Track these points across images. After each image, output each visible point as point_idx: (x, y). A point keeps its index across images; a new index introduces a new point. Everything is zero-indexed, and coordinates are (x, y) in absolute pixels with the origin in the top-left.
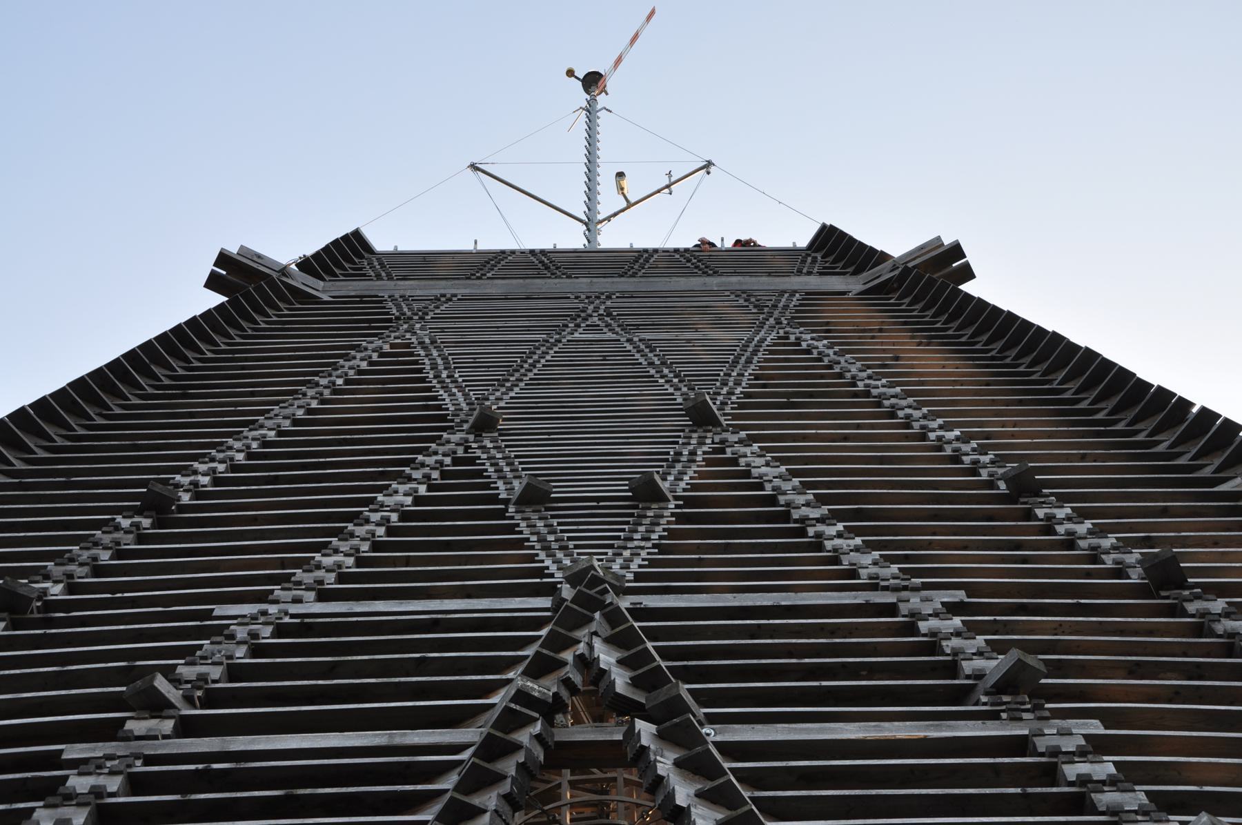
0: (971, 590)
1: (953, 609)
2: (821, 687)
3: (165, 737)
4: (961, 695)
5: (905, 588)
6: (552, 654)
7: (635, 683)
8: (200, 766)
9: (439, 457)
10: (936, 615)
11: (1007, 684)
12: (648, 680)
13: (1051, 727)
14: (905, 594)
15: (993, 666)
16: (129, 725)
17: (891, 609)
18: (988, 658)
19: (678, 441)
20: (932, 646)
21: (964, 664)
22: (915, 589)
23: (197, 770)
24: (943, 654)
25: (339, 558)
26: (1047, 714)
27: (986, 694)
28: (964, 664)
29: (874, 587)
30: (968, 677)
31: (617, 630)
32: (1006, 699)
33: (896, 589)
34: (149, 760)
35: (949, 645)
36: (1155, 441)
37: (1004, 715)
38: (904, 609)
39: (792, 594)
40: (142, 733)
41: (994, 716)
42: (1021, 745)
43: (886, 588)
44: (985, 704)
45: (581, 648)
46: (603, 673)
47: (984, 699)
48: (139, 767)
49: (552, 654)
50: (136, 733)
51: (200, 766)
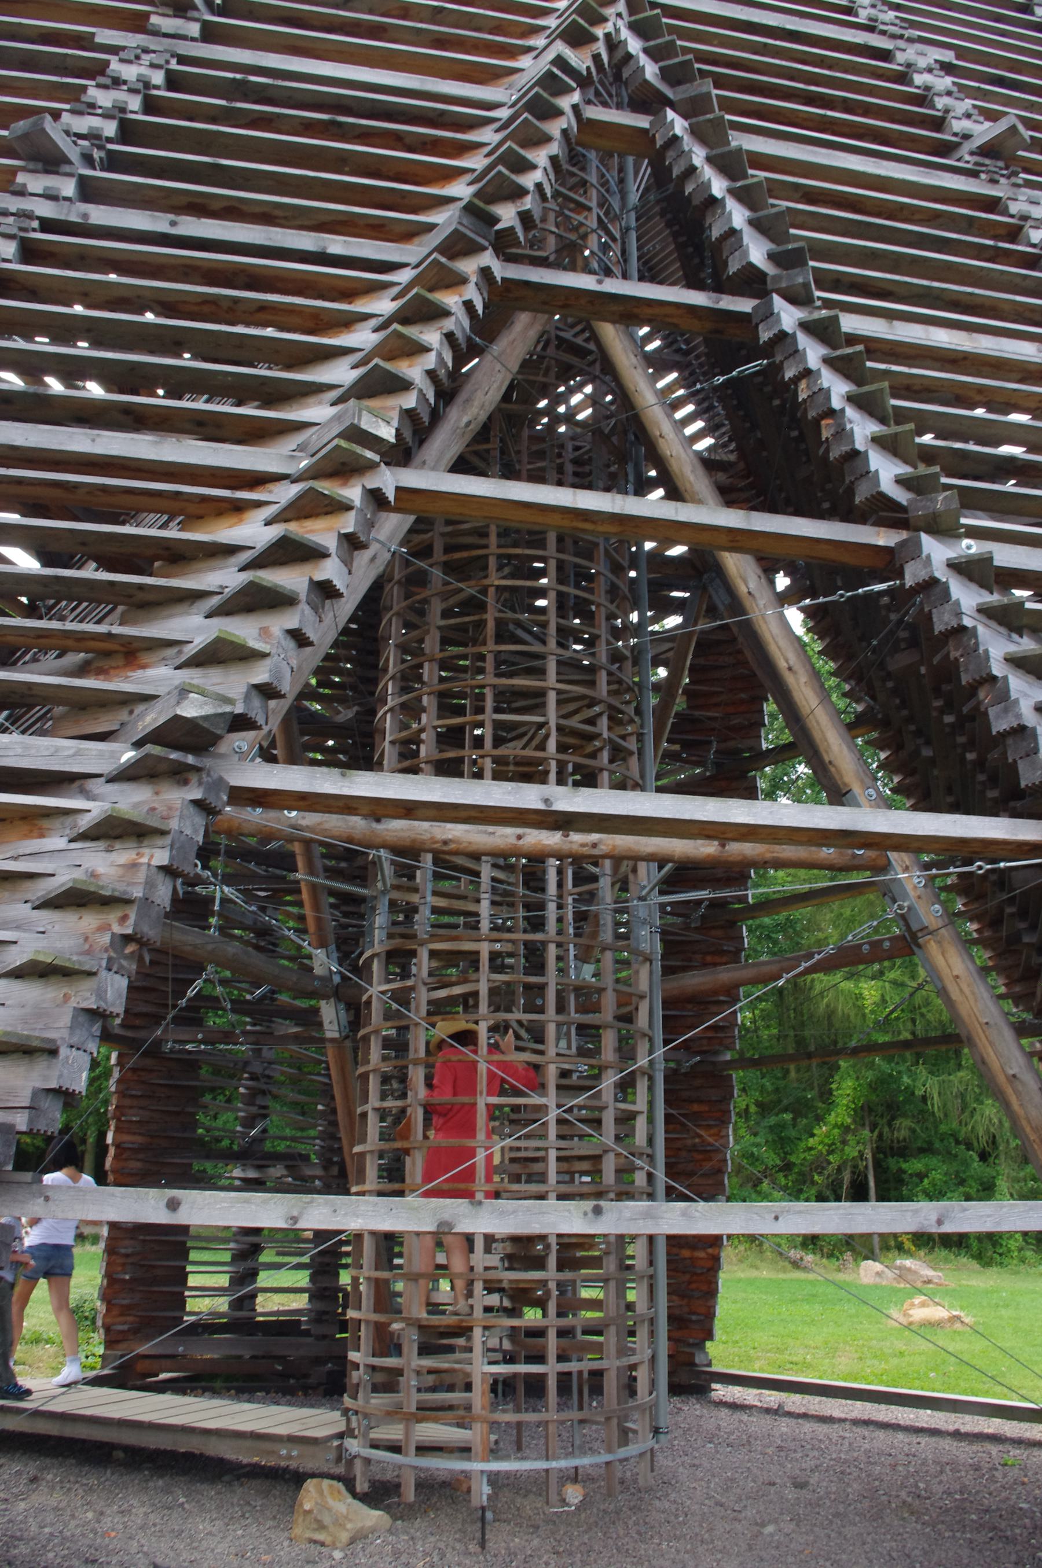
0: (962, 53)
1: (947, 68)
2: (824, 116)
3: (193, 39)
4: (945, 149)
5: (901, 37)
6: (586, 25)
7: (665, 74)
8: (238, 76)
9: (144, 70)
10: (930, 70)
11: (988, 150)
12: (673, 76)
13: (1024, 194)
14: (901, 44)
15: (984, 131)
16: (154, 20)
17: (885, 55)
18: (975, 121)
19: (179, 63)
20: (923, 99)
21: (954, 122)
22: (911, 40)
23: (234, 80)
24: (933, 108)
25: (120, 95)
26: (1021, 182)
27: (972, 153)
28: (954, 122)
29: (870, 29)
30: (955, 135)
31: (638, 17)
32: (987, 161)
33: (893, 37)
34: (182, 60)
35: (940, 102)
36: (538, 26)
37: (983, 176)
38: (900, 57)
39: (797, 19)
40: (171, 31)
41: (973, 174)
42: (992, 204)
43: (883, 33)
44: (968, 162)
45: (609, 27)
46: (629, 57)
47: (967, 158)
48: (174, 65)
49: (586, 25)
50: (164, 31)
51: (238, 76)
